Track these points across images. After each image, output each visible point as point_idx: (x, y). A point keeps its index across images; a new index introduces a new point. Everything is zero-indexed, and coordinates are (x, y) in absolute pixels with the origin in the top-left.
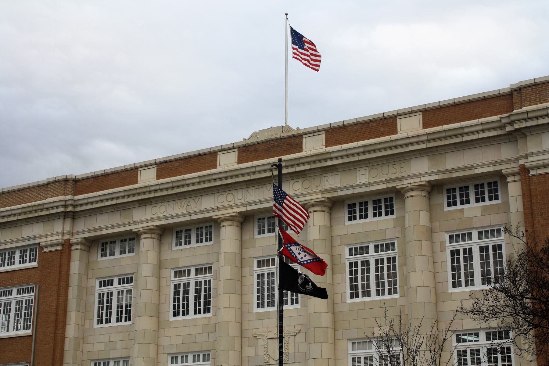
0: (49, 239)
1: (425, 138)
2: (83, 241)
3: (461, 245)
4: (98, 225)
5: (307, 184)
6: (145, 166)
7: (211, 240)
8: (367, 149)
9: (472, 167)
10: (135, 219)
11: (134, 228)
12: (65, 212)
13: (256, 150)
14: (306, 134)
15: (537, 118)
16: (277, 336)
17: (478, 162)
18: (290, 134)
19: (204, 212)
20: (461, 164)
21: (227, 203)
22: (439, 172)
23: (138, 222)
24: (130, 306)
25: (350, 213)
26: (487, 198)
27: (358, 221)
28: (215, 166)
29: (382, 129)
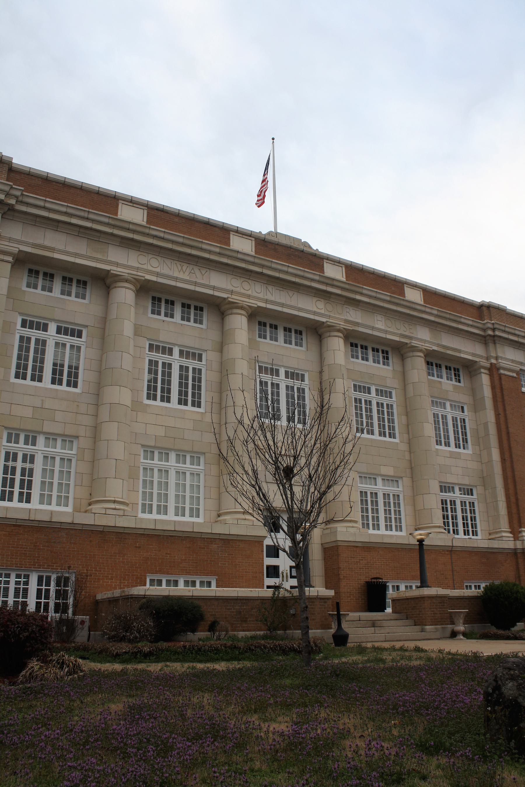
9: (459, 351)
16: (66, 433)
24: (77, 368)
29: (393, 289)
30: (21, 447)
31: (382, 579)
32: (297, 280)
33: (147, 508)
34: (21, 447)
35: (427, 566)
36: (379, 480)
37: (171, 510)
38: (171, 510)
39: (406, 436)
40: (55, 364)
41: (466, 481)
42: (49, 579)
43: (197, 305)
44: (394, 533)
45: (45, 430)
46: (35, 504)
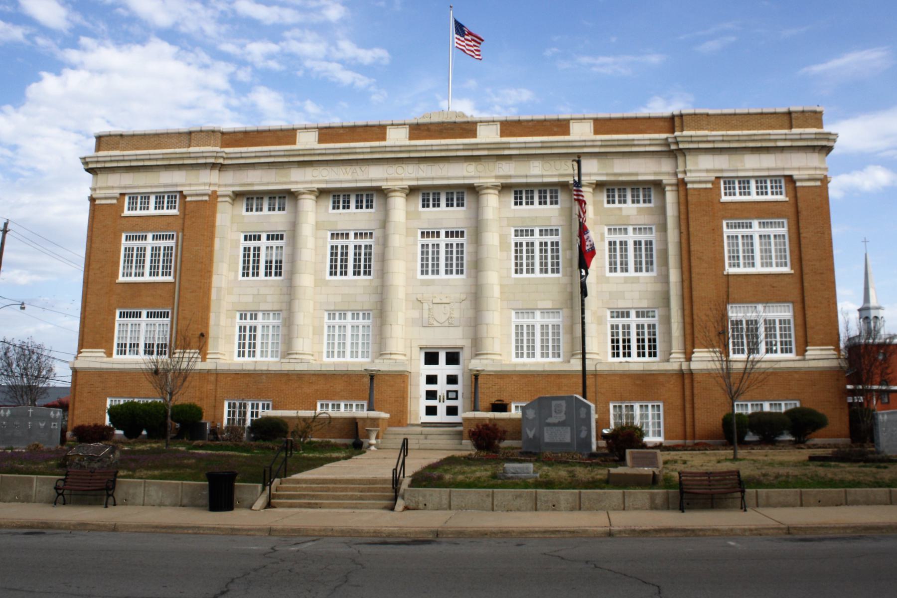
0: (193, 188)
1: (599, 143)
2: (231, 194)
3: (618, 238)
4: (249, 181)
5: (547, 166)
6: (305, 128)
7: (372, 207)
8: (545, 145)
10: (293, 179)
11: (293, 187)
12: (214, 164)
13: (428, 130)
14: (481, 122)
15: (699, 142)
17: (642, 170)
18: (465, 120)
19: (371, 180)
20: (627, 171)
21: (397, 176)
22: (607, 174)
23: (297, 183)
24: (281, 262)
25: (516, 198)
26: (641, 201)
27: (524, 206)
28: (294, 143)
30: (248, 322)
33: (330, 354)
34: (248, 322)
36: (538, 313)
37: (348, 353)
38: (348, 353)
39: (568, 269)
40: (267, 262)
41: (644, 304)
42: (257, 405)
43: (369, 196)
46: (258, 358)
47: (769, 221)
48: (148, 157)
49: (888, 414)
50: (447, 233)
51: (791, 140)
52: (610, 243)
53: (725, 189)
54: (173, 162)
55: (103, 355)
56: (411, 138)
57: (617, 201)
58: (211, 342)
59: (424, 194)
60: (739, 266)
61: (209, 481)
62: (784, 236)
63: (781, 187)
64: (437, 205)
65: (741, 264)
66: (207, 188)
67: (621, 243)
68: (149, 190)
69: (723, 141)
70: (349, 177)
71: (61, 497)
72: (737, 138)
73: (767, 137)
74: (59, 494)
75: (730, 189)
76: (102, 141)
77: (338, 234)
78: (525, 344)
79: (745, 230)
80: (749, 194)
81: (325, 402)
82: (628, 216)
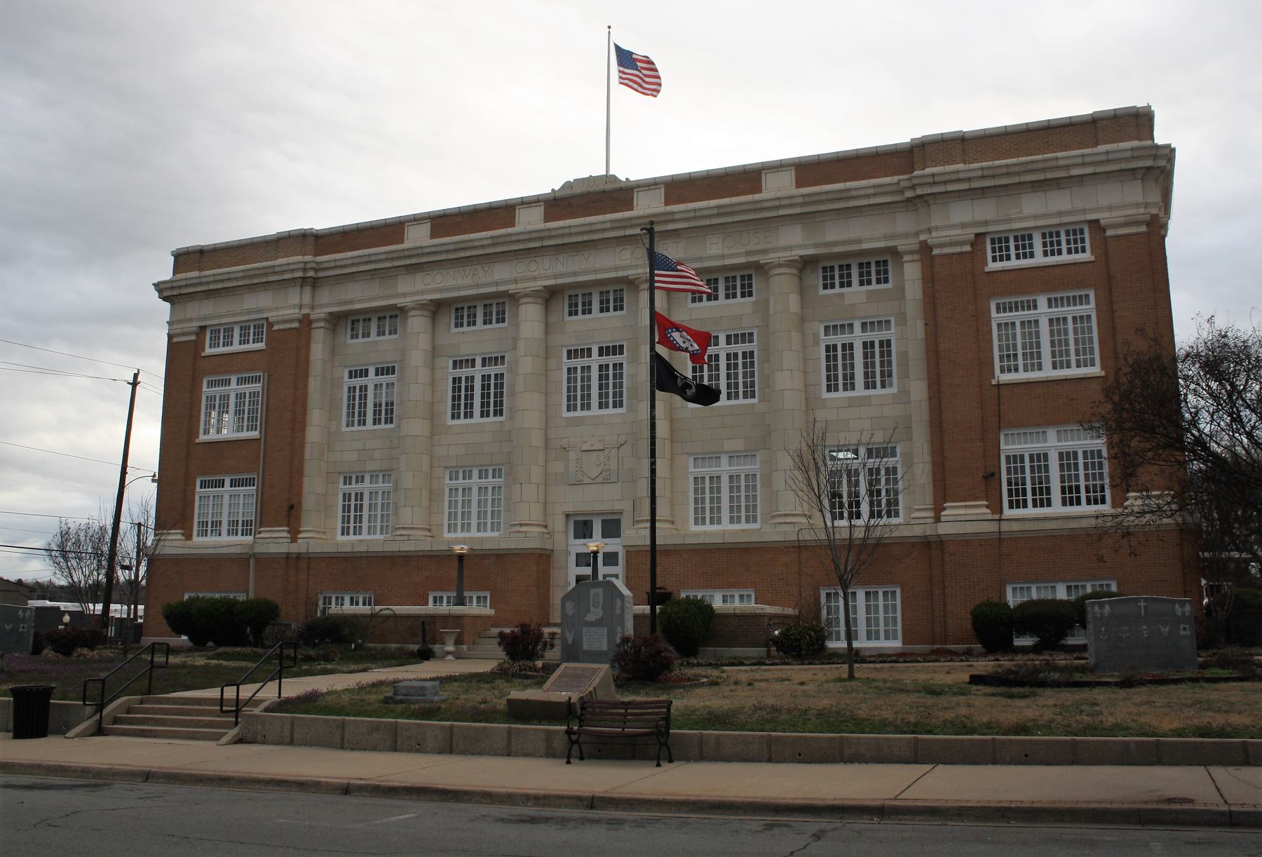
3: (839, 339)
4: (348, 297)
8: (722, 210)
9: (859, 241)
10: (401, 290)
12: (1149, 169)
15: (945, 183)
18: (617, 186)
20: (845, 237)
23: (405, 295)
24: (392, 404)
31: (1191, 801)
32: (586, 238)
35: (648, 574)
38: (365, 529)
44: (1030, 511)
45: (726, 449)
47: (1077, 293)
48: (226, 277)
49: (1110, 603)
50: (601, 349)
51: (1093, 164)
52: (828, 348)
53: (994, 250)
54: (256, 281)
55: (179, 537)
56: (546, 220)
57: (837, 285)
58: (305, 517)
59: (824, 269)
60: (1016, 370)
61: (14, 697)
62: (1089, 317)
63: (1083, 241)
64: (367, 334)
65: (1021, 368)
66: (1142, 211)
67: (881, 343)
68: (1032, 224)
69: (983, 177)
70: (468, 281)
71: (576, 747)
72: (1004, 170)
73: (1054, 163)
74: (573, 743)
75: (1001, 249)
76: (184, 259)
77: (461, 361)
78: (708, 506)
79: (1026, 312)
80: (1032, 255)
81: (438, 594)
82: (854, 305)
